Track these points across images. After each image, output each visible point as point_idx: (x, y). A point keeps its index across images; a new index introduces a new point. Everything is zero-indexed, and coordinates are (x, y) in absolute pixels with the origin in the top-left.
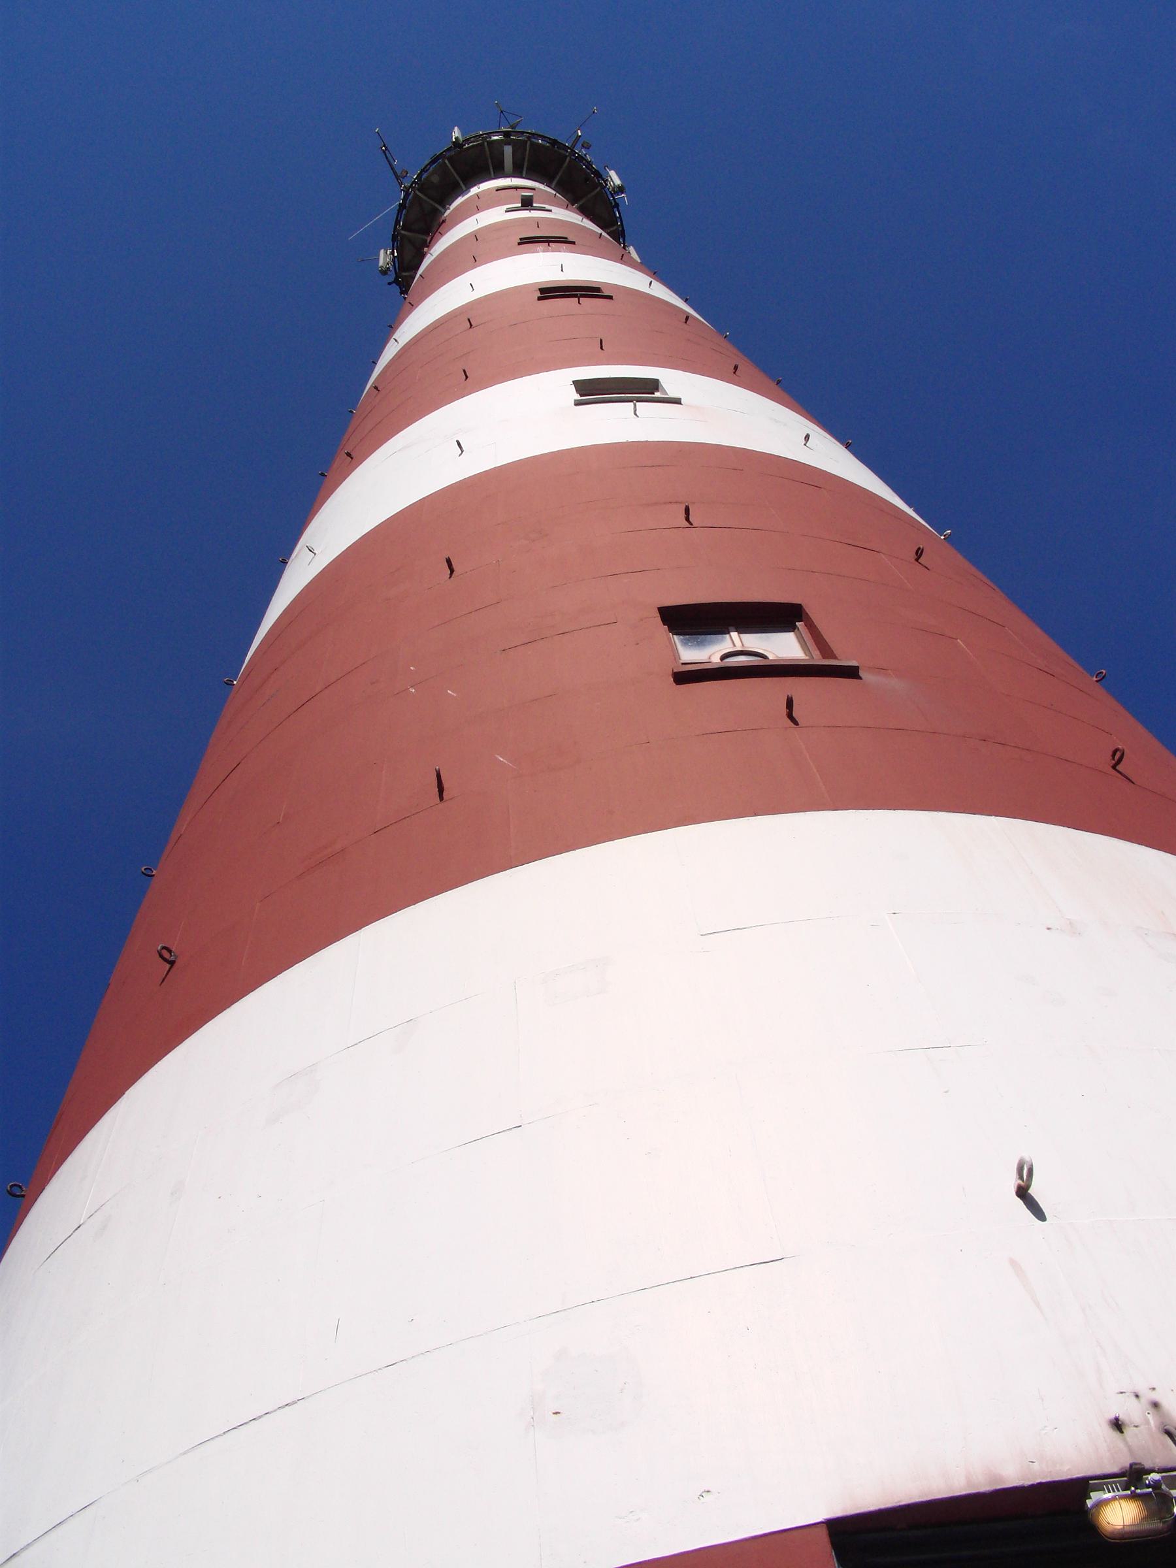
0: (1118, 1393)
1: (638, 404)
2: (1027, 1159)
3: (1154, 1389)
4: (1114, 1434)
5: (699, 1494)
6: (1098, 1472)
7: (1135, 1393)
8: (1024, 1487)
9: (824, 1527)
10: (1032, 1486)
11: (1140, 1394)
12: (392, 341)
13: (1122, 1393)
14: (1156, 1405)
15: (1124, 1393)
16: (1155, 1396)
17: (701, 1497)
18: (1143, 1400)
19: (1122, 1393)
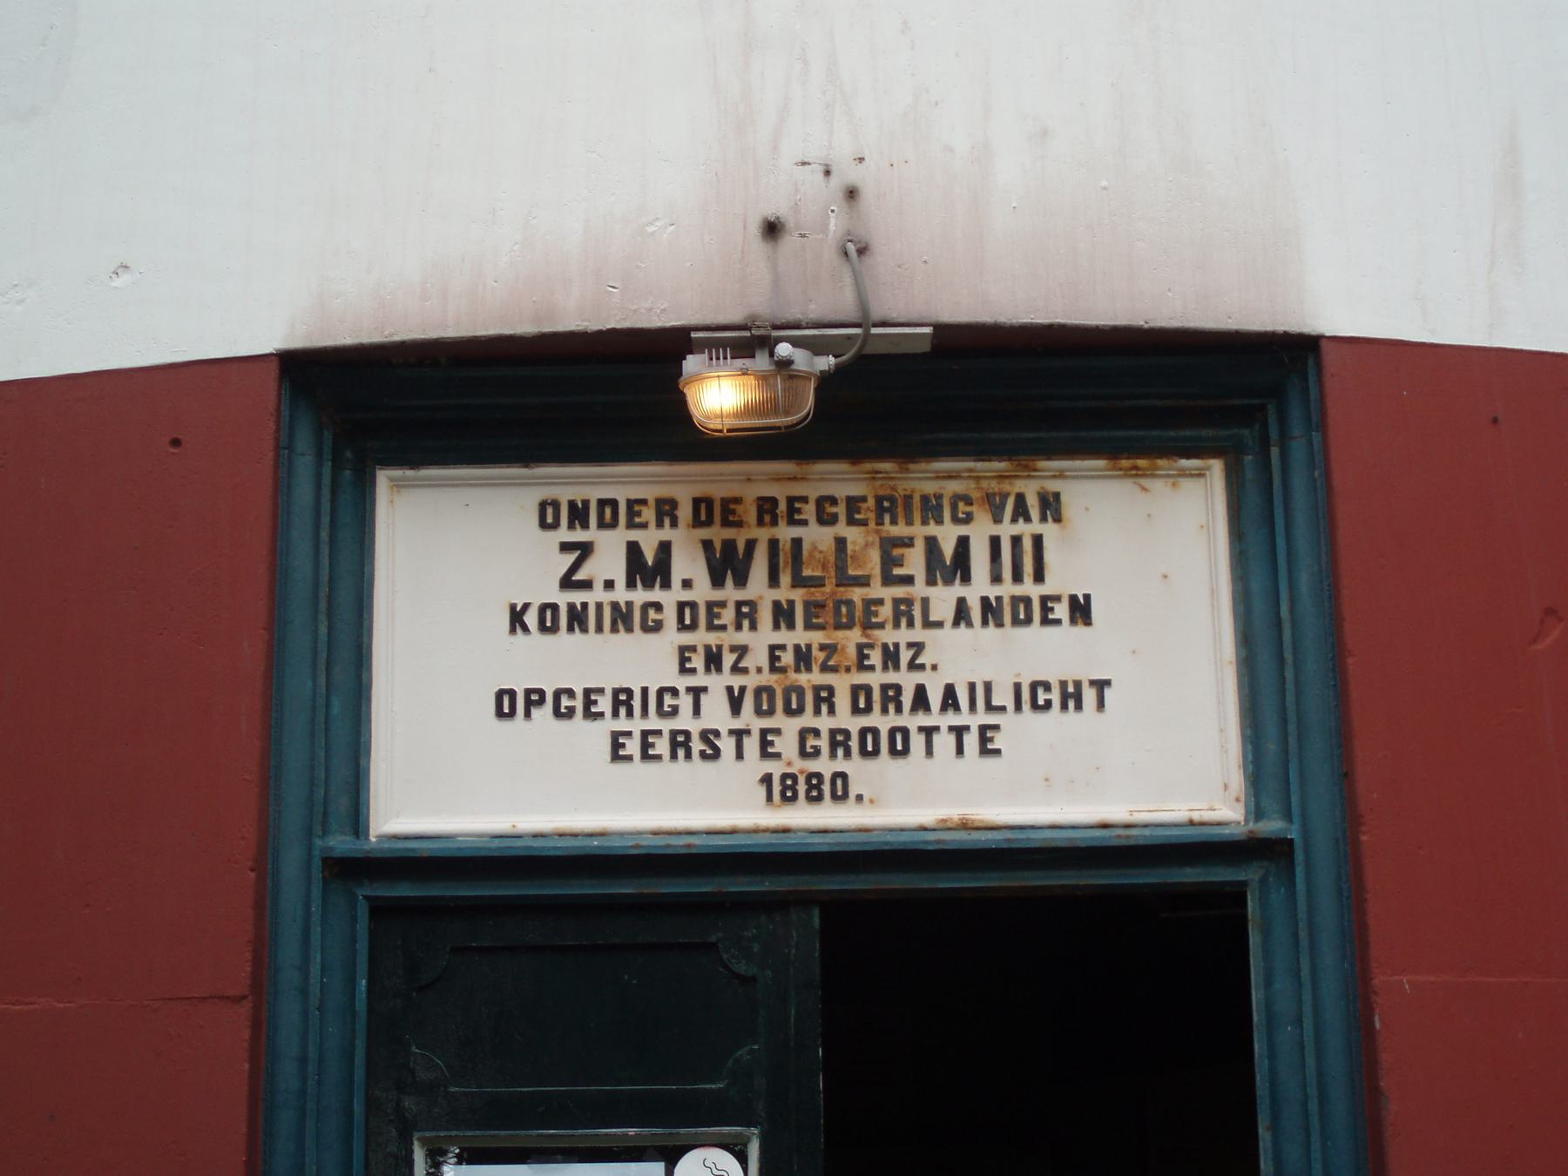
0: (797, 164)
1: (245, 1008)
2: (1009, 631)
3: (861, 160)
4: (756, 245)
5: (112, 270)
6: (710, 319)
7: (827, 165)
8: (586, 332)
9: (277, 358)
10: (600, 332)
11: (834, 170)
12: (1243, 798)
13: (804, 164)
14: (852, 194)
15: (809, 164)
16: (854, 175)
17: (114, 276)
18: (835, 180)
19: (804, 164)
